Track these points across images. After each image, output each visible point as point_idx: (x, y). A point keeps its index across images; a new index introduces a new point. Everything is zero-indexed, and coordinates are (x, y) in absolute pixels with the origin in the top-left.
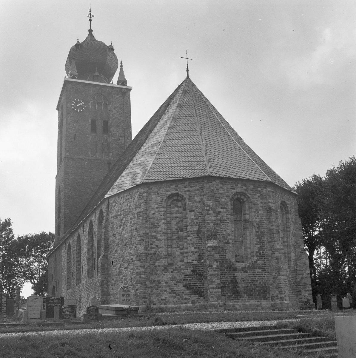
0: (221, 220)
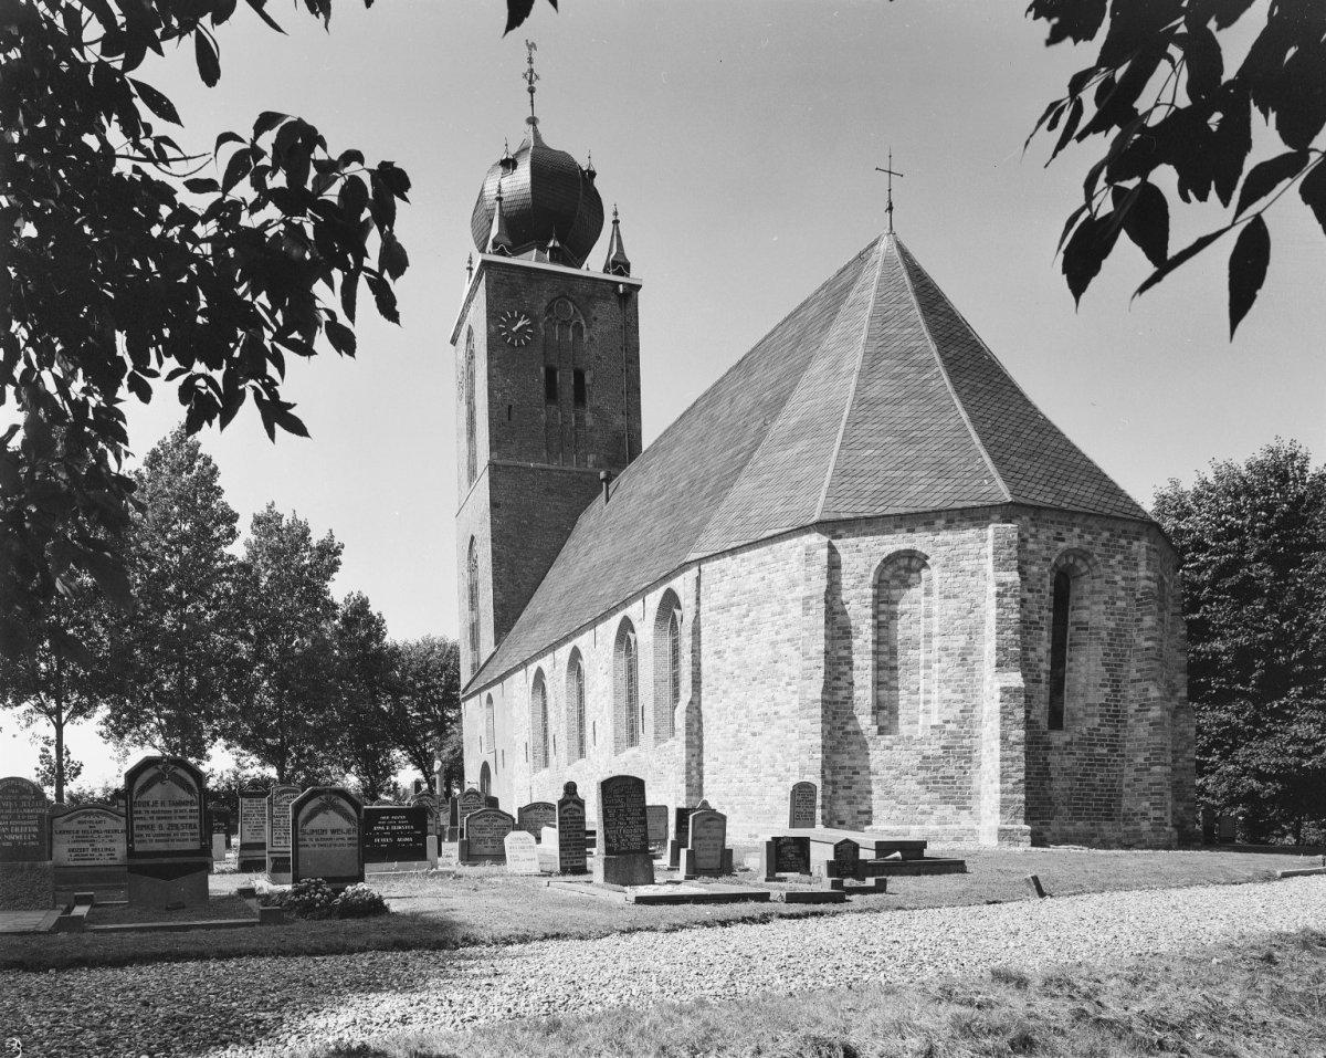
0: (1026, 622)
